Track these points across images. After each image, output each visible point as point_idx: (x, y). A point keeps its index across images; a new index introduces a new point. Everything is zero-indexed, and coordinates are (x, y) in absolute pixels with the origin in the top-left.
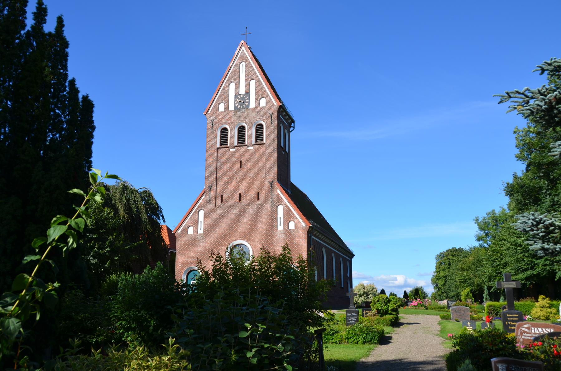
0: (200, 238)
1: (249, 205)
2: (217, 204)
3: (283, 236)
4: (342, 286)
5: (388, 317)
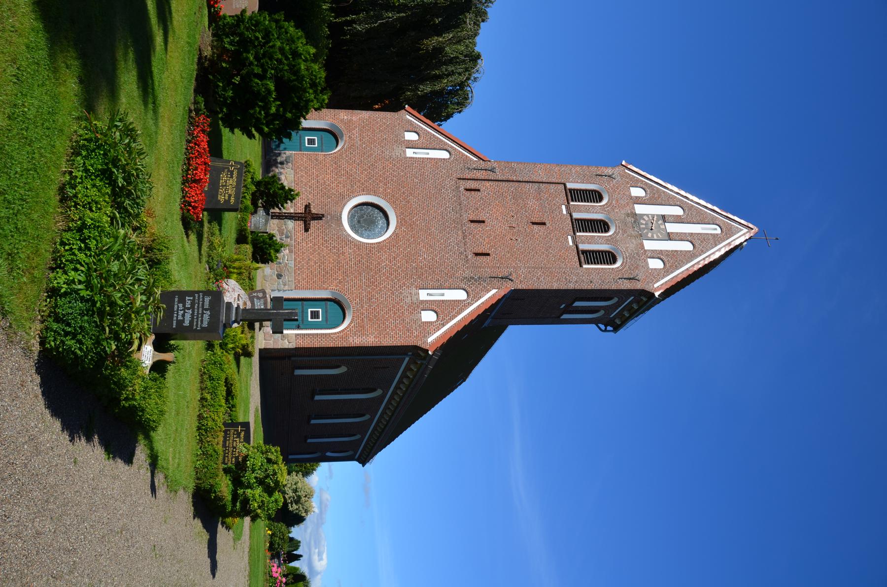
0: (397, 152)
1: (464, 237)
2: (462, 182)
3: (408, 300)
4: (309, 441)
5: (224, 487)
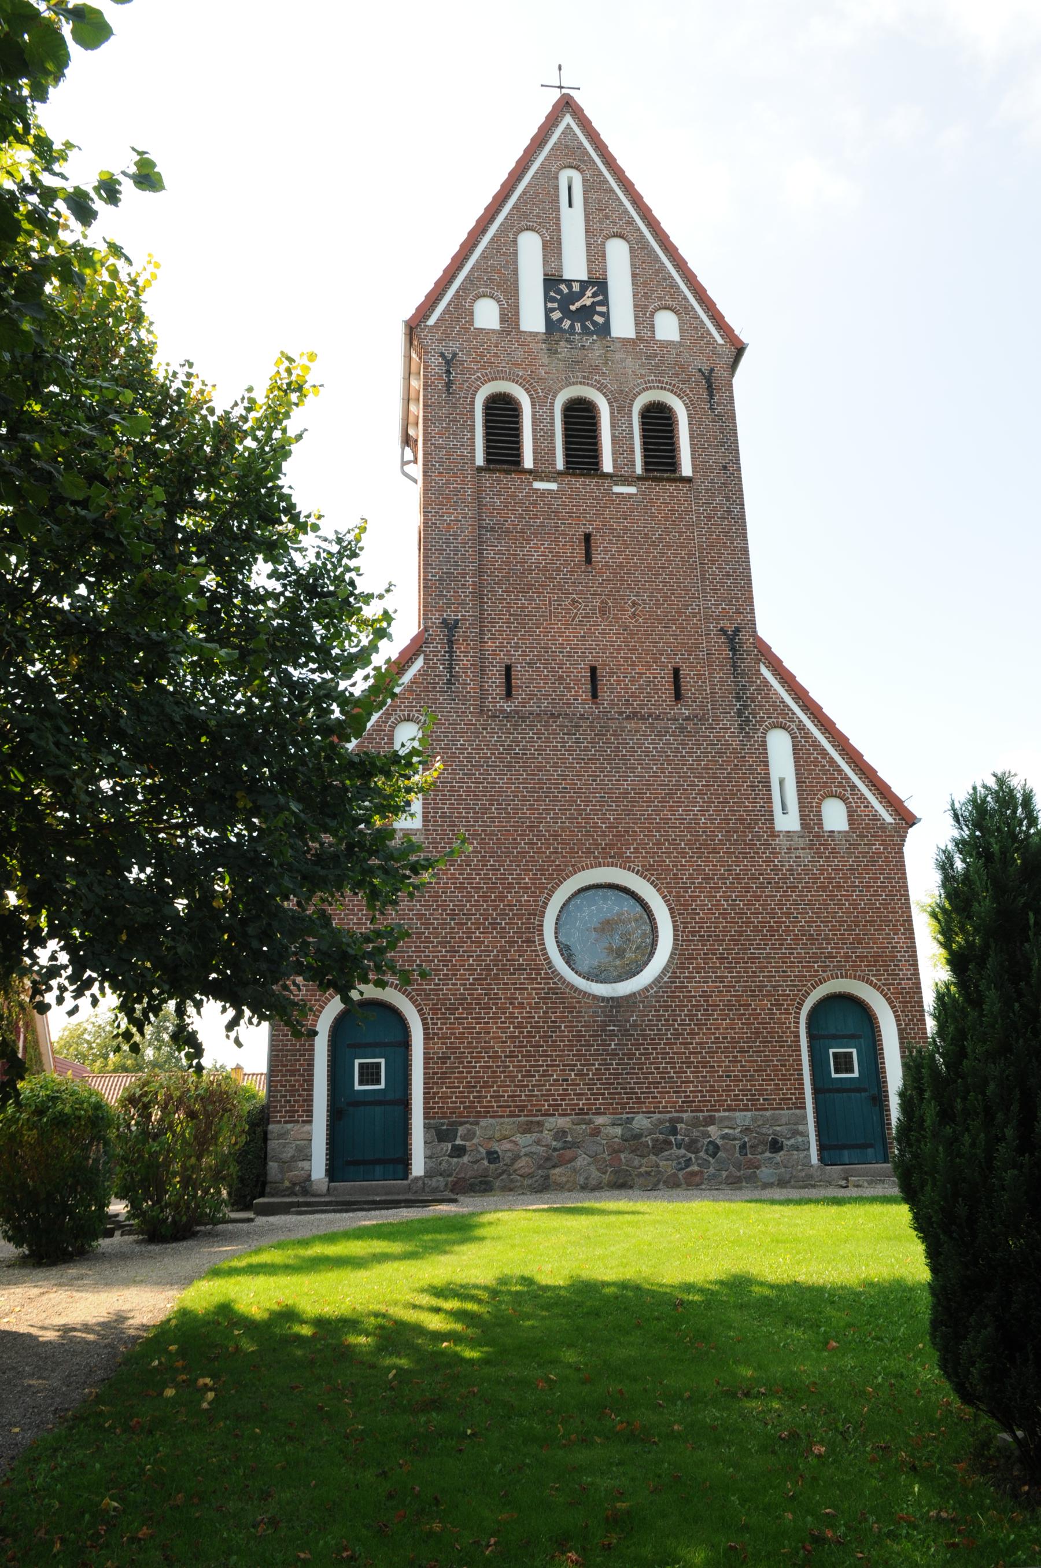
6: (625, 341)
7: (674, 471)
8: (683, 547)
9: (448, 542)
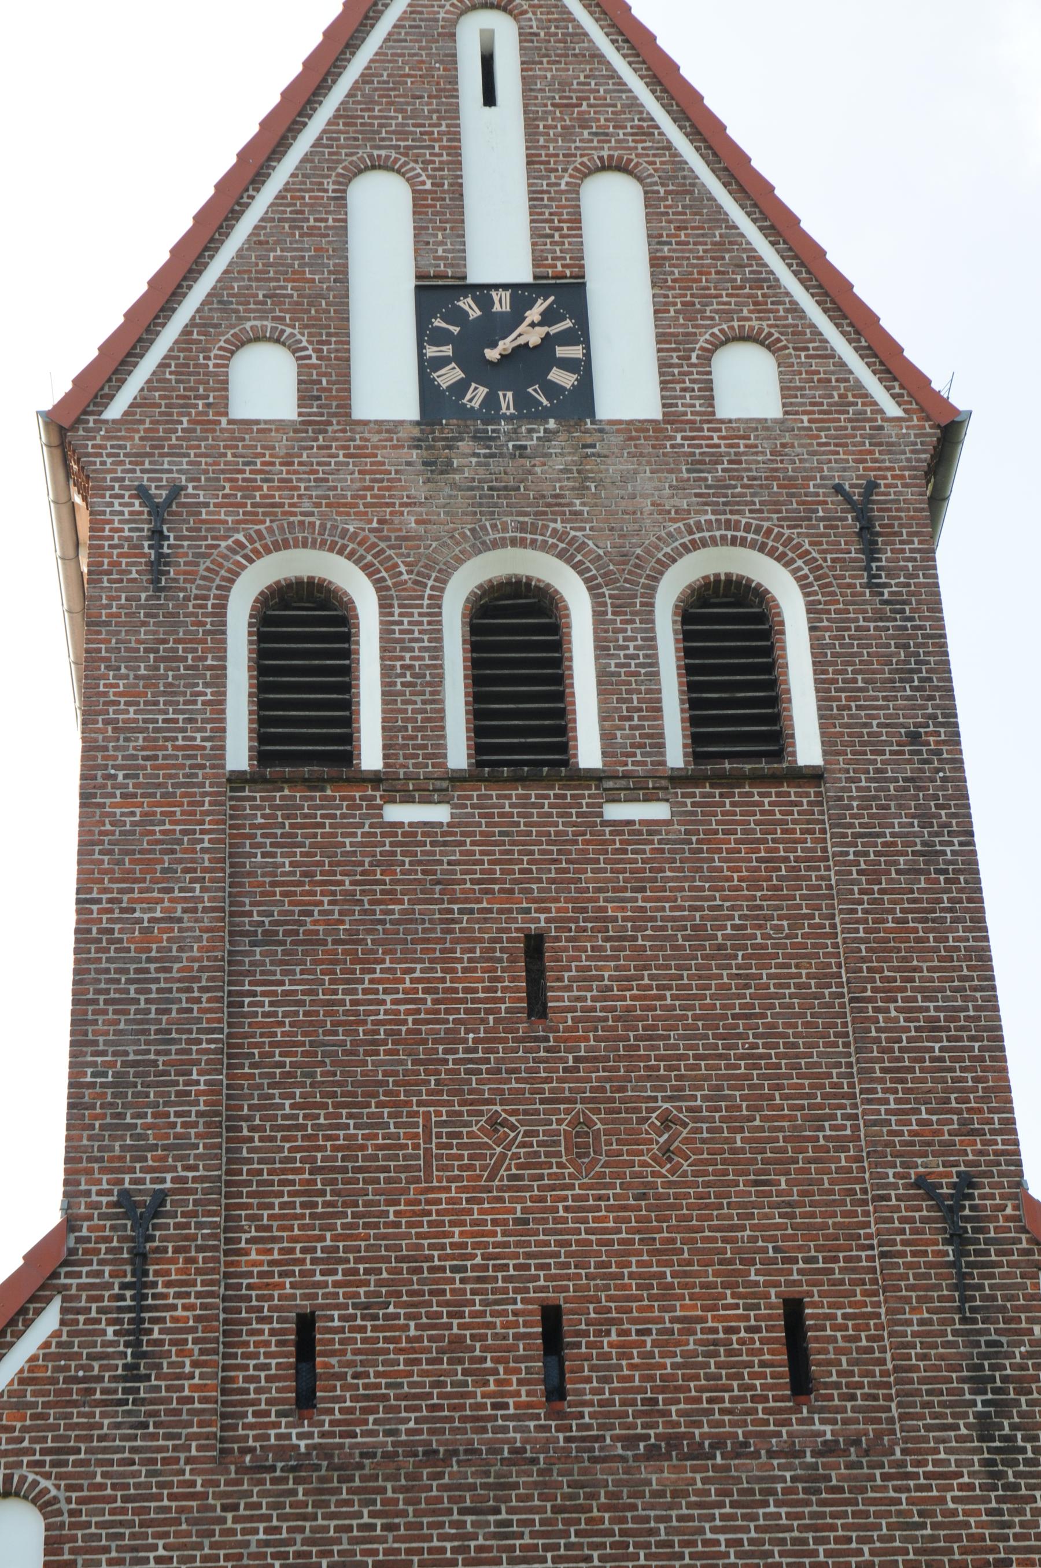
1: (672, 1446)
6: (633, 430)
7: (778, 755)
8: (804, 957)
9: (142, 980)
